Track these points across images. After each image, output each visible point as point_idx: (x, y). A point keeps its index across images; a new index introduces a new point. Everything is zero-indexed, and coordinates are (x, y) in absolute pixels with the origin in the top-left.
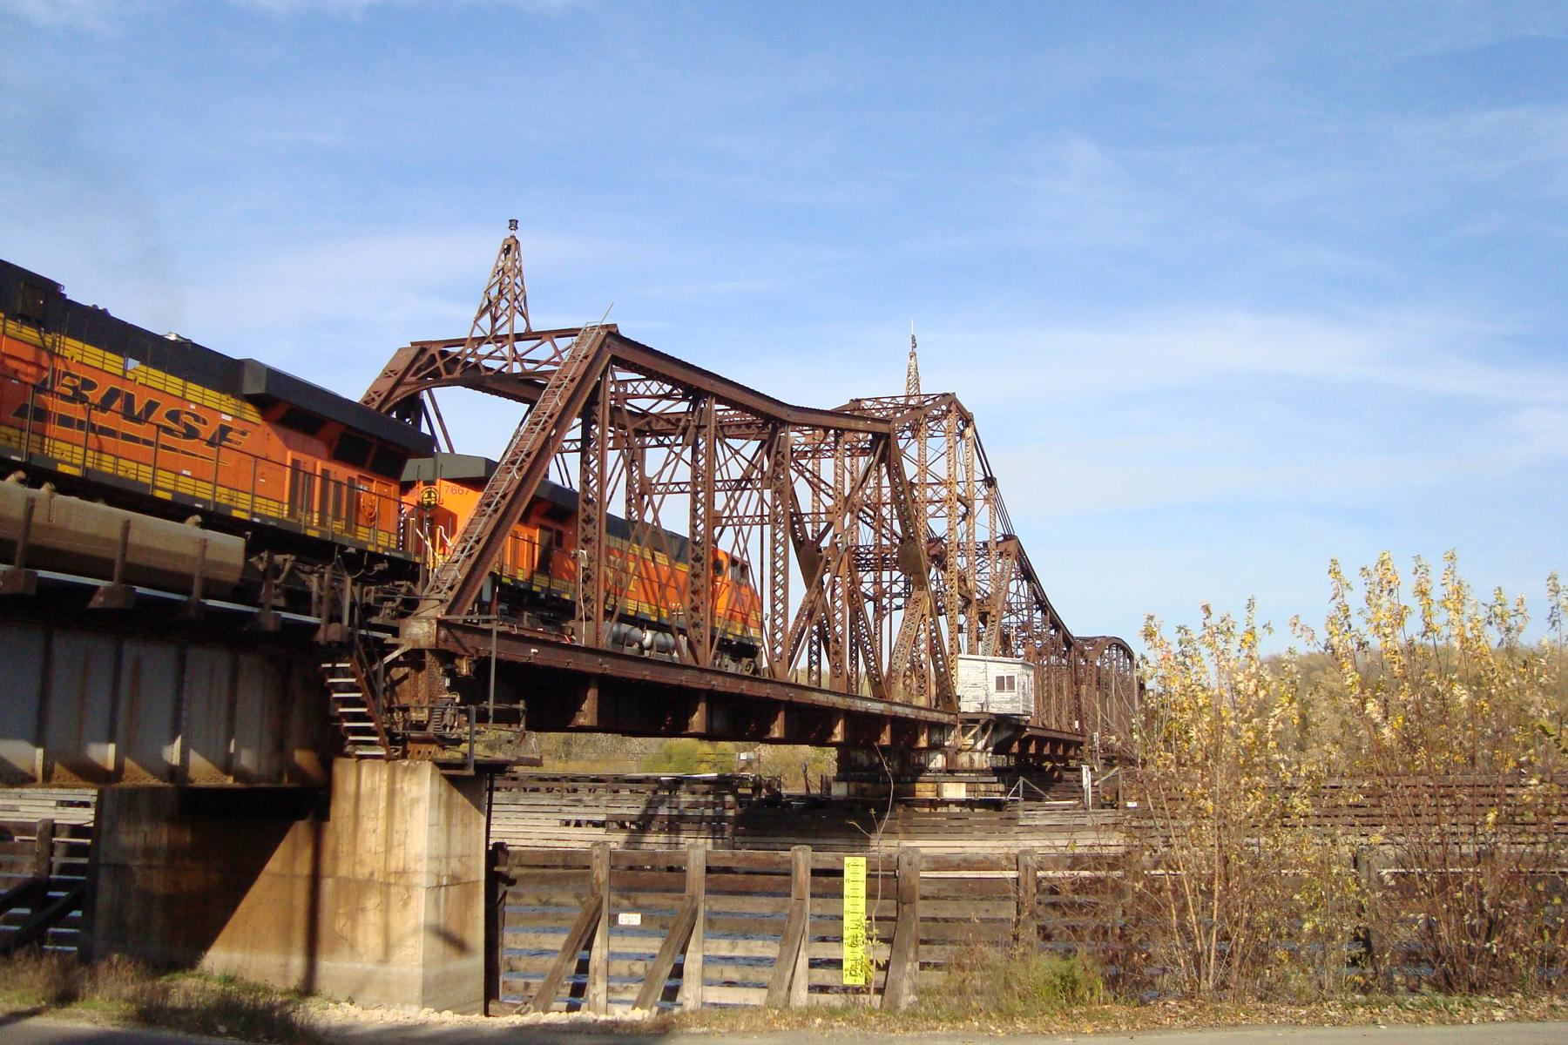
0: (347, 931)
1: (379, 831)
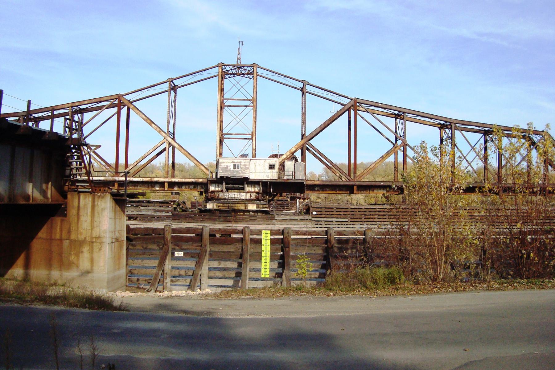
0: (76, 262)
1: (88, 221)
